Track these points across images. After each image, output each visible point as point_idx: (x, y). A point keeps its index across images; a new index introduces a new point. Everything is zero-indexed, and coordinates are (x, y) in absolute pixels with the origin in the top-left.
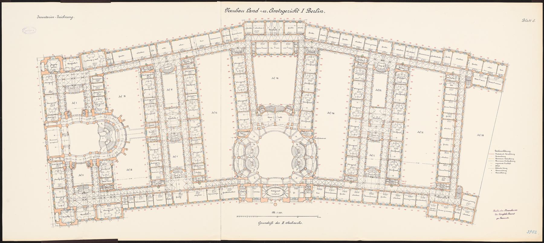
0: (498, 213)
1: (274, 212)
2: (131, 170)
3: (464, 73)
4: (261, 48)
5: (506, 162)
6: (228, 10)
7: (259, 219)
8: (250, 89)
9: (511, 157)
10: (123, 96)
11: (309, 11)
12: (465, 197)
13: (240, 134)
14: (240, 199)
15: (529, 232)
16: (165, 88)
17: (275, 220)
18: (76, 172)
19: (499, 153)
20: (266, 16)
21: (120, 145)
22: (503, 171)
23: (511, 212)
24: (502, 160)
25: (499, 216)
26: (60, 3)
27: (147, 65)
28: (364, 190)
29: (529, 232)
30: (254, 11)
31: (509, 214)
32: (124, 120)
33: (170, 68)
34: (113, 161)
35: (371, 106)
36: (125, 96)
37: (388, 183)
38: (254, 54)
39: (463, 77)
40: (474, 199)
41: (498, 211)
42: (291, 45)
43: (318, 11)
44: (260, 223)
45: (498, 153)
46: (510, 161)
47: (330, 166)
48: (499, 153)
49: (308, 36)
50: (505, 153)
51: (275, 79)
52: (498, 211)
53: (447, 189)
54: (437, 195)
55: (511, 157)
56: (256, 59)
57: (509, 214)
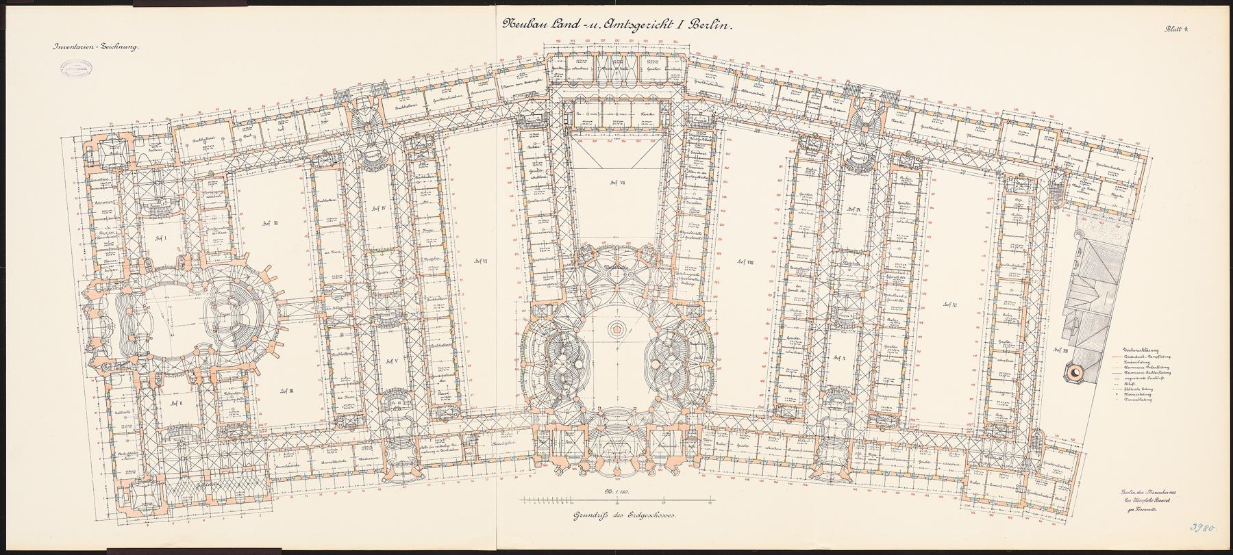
0: (1131, 497)
1: (609, 491)
2: (291, 391)
4: (584, 114)
6: (509, 22)
7: (577, 507)
8: (563, 211)
9: (1161, 362)
10: (272, 223)
11: (696, 23)
14: (538, 459)
15: (1196, 527)
17: (612, 508)
18: (164, 401)
19: (1134, 354)
20: (596, 35)
21: (266, 336)
22: (1145, 396)
25: (1134, 505)
26: (129, 9)
29: (1196, 527)
30: (571, 26)
31: (1157, 500)
34: (246, 372)
35: (837, 250)
36: (276, 223)
39: (1048, 178)
40: (1069, 460)
41: (1132, 492)
42: (654, 108)
43: (716, 25)
44: (577, 516)
45: (1129, 354)
46: (1161, 373)
47: (741, 382)
48: (1134, 354)
49: (693, 88)
51: (619, 192)
52: (1132, 492)
53: (1010, 441)
54: (986, 453)
55: (1161, 362)
57: (1157, 500)
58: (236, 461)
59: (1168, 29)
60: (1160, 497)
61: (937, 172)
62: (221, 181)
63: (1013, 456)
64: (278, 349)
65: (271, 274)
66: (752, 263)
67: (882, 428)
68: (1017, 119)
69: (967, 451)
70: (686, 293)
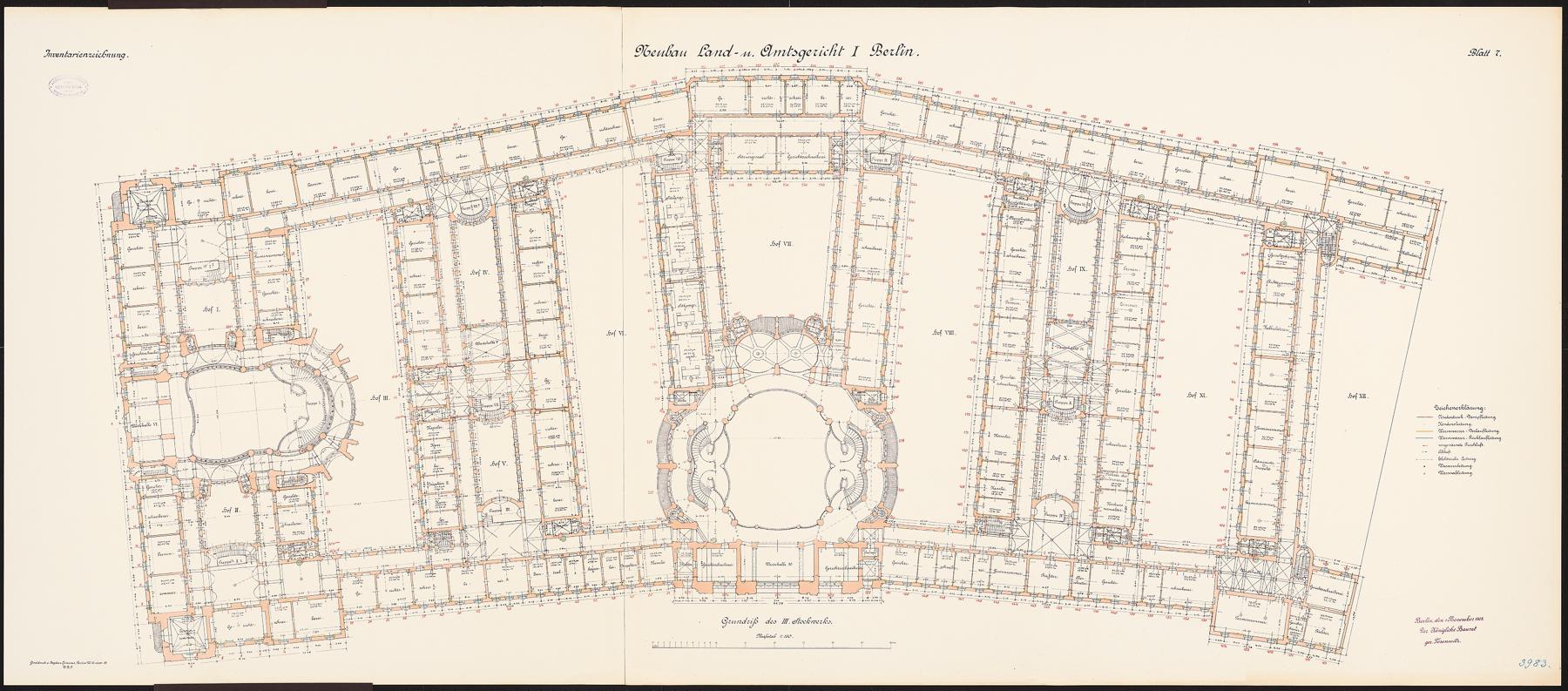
0: (1428, 626)
3: (1314, 225)
5: (1471, 442)
12: (1318, 579)
13: (680, 398)
16: (465, 269)
23: (1466, 625)
24: (1462, 430)
25: (1432, 637)
26: (103, 11)
27: (411, 203)
28: (1028, 555)
30: (719, 53)
31: (1461, 629)
32: (348, 360)
33: (477, 210)
37: (1099, 539)
38: (716, 171)
40: (1344, 585)
47: (933, 491)
50: (1465, 413)
51: (775, 240)
56: (722, 185)
57: (1461, 629)
58: (1252, 582)
59: (1474, 52)
60: (1464, 625)
61: (919, 174)
62: (280, 240)
63: (1234, 574)
64: (351, 449)
65: (342, 355)
66: (951, 333)
67: (1109, 544)
68: (1407, 190)
69: (1216, 572)
70: (863, 372)
